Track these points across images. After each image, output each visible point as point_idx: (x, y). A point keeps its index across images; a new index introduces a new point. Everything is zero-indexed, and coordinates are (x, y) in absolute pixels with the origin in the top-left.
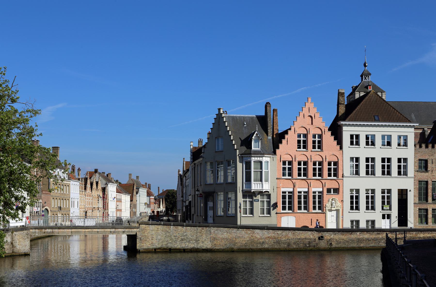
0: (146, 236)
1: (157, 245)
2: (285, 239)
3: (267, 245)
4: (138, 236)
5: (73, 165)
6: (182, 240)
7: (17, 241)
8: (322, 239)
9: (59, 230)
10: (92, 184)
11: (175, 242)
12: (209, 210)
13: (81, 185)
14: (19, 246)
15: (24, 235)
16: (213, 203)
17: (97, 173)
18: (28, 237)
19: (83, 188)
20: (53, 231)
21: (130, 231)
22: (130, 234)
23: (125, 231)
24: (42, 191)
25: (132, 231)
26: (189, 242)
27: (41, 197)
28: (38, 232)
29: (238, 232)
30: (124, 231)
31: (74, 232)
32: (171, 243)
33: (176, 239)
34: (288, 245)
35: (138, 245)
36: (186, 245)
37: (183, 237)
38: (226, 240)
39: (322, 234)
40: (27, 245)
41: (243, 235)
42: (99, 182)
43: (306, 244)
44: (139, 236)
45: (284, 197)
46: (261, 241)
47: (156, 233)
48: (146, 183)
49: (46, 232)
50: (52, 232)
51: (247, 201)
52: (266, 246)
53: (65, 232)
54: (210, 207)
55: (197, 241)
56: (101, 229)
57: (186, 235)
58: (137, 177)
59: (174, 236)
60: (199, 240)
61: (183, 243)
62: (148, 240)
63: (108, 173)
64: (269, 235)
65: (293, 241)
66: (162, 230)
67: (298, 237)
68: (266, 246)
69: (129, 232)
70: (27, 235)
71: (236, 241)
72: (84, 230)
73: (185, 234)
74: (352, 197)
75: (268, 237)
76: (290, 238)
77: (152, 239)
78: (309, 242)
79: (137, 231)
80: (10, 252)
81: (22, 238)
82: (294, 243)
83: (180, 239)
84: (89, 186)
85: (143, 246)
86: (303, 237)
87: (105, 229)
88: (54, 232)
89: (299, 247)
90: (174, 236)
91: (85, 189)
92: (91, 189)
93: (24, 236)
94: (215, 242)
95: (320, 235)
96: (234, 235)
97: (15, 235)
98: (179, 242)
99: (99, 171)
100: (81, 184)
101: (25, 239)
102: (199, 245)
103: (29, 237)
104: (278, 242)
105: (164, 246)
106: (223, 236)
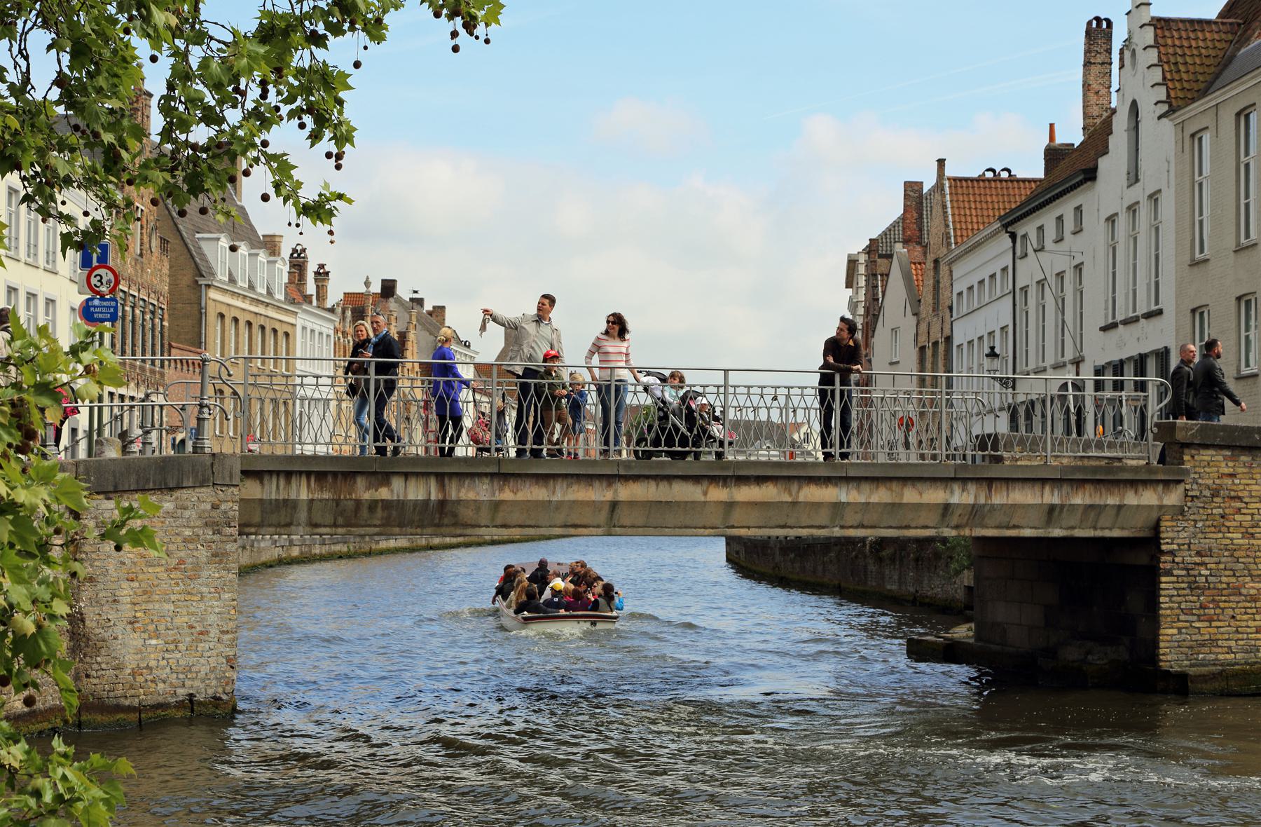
0: (1232, 550)
4: (1172, 553)
5: (299, 248)
7: (125, 585)
9: (501, 490)
13: (339, 339)
14: (135, 640)
15: (188, 532)
17: (391, 300)
18: (226, 554)
20: (454, 496)
21: (1106, 506)
22: (1099, 533)
23: (1062, 506)
24: (166, 346)
25: (1120, 508)
27: (162, 375)
28: (311, 501)
31: (631, 504)
40: (214, 632)
44: (1173, 536)
49: (387, 504)
50: (442, 503)
53: (560, 504)
56: (866, 487)
63: (434, 307)
69: (1092, 515)
70: (215, 526)
79: (1161, 507)
85: (1213, 642)
87: (895, 485)
88: (459, 502)
99: (403, 292)
100: (340, 335)
101: (197, 567)
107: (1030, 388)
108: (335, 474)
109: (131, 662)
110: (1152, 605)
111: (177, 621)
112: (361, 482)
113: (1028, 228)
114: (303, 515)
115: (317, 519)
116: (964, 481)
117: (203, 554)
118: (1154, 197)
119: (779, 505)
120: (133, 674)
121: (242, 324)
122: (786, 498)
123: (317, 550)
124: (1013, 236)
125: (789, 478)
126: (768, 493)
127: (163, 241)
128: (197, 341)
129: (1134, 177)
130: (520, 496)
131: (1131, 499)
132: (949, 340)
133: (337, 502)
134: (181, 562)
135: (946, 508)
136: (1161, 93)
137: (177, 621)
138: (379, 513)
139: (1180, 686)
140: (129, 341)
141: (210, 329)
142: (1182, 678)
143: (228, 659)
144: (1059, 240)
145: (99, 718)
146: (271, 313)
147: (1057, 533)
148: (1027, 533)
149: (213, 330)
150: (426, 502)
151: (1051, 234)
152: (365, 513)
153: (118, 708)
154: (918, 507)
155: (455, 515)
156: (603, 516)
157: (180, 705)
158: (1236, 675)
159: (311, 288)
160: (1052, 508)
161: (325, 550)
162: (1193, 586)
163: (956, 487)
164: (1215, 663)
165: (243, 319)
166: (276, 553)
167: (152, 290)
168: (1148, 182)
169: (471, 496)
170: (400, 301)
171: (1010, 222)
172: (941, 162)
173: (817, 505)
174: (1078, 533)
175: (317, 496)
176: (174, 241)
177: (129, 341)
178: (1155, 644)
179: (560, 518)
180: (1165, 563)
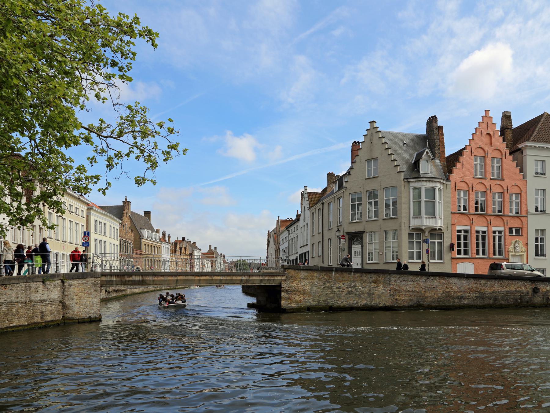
1: (312, 302)
2: (490, 291)
3: (467, 300)
6: (349, 293)
8: (537, 291)
10: (181, 249)
11: (339, 296)
12: (355, 255)
14: (77, 306)
15: (89, 286)
16: (362, 246)
19: (174, 251)
25: (274, 280)
26: (359, 296)
29: (428, 281)
30: (262, 279)
32: (332, 298)
33: (340, 293)
34: (495, 301)
35: (283, 302)
36: (354, 301)
37: (350, 289)
38: (411, 293)
39: (536, 285)
40: (95, 305)
41: (435, 286)
42: (187, 248)
43: (516, 300)
44: (284, 285)
45: (459, 238)
46: (459, 294)
47: (309, 283)
48: (221, 254)
50: (143, 280)
51: (413, 242)
52: (466, 302)
53: (166, 280)
54: (355, 252)
55: (370, 295)
56: (226, 277)
57: (355, 286)
58: (215, 248)
59: (337, 288)
60: (373, 294)
61: (350, 298)
62: (298, 293)
64: (470, 286)
65: (500, 295)
66: (319, 279)
67: (507, 289)
68: (466, 302)
70: (95, 285)
71: (426, 295)
72: (197, 278)
73: (353, 284)
74: (537, 239)
75: (468, 289)
76: (496, 291)
77: (305, 293)
78: (521, 296)
80: (57, 318)
81: (84, 290)
82: (503, 297)
83: (345, 292)
84: (178, 250)
85: (291, 303)
86: (513, 289)
87: (231, 276)
89: (508, 302)
90: (337, 288)
91: (175, 252)
92: (181, 253)
93: (88, 288)
94: (397, 297)
95: (534, 286)
96: (423, 286)
97: (70, 285)
98: (344, 296)
99: (186, 239)
101: (91, 293)
102: (374, 301)
103: (98, 289)
104: (482, 296)
105: (322, 303)
106: (407, 288)
107: (291, 258)
108: (121, 275)
109: (76, 310)
110: (281, 297)
111: (87, 303)
112: (126, 277)
113: (290, 229)
114: (115, 283)
115: (118, 283)
116: (245, 275)
117: (92, 290)
118: (307, 224)
119: (209, 280)
120: (77, 313)
121: (150, 246)
122: (211, 279)
123: (163, 288)
124: (288, 231)
125: (211, 275)
126: (207, 278)
127: (132, 230)
128: (140, 249)
129: (304, 221)
130: (158, 279)
131: (276, 278)
132: (280, 249)
133: (121, 280)
134: (87, 292)
135: (241, 280)
136: (308, 206)
137: (87, 303)
138: (130, 282)
139: (285, 311)
140: (124, 249)
141: (143, 247)
142: (285, 309)
143: (98, 310)
144: (294, 231)
145: (69, 321)
146: (156, 244)
147: (263, 284)
148: (257, 284)
149: (143, 247)
150: (139, 280)
151: (293, 230)
152: (127, 282)
153: (73, 319)
154: (236, 280)
155: (145, 282)
156: (175, 282)
157: (87, 318)
158: (295, 309)
159: (167, 239)
160: (261, 280)
161: (165, 288)
162: (287, 294)
163: (243, 277)
164: (291, 307)
165: (150, 245)
166: (154, 289)
167: (129, 239)
168: (306, 222)
169: (149, 279)
170: (186, 241)
171: (287, 228)
172: (279, 217)
173: (217, 280)
174: (267, 284)
175: (117, 279)
176: (135, 230)
177: (124, 249)
178: (281, 304)
179: (167, 283)
180: (282, 289)
